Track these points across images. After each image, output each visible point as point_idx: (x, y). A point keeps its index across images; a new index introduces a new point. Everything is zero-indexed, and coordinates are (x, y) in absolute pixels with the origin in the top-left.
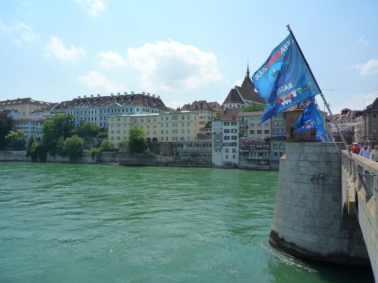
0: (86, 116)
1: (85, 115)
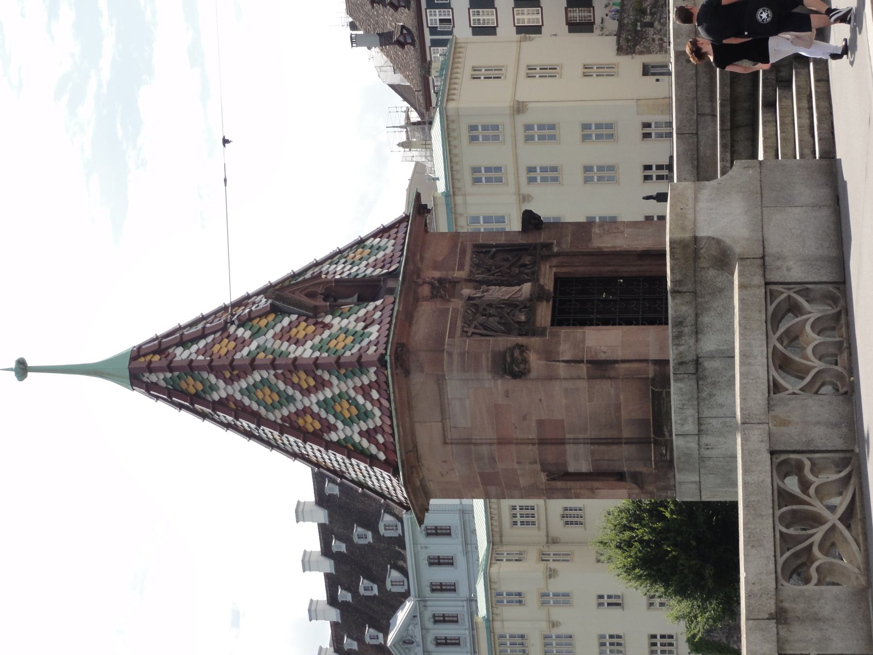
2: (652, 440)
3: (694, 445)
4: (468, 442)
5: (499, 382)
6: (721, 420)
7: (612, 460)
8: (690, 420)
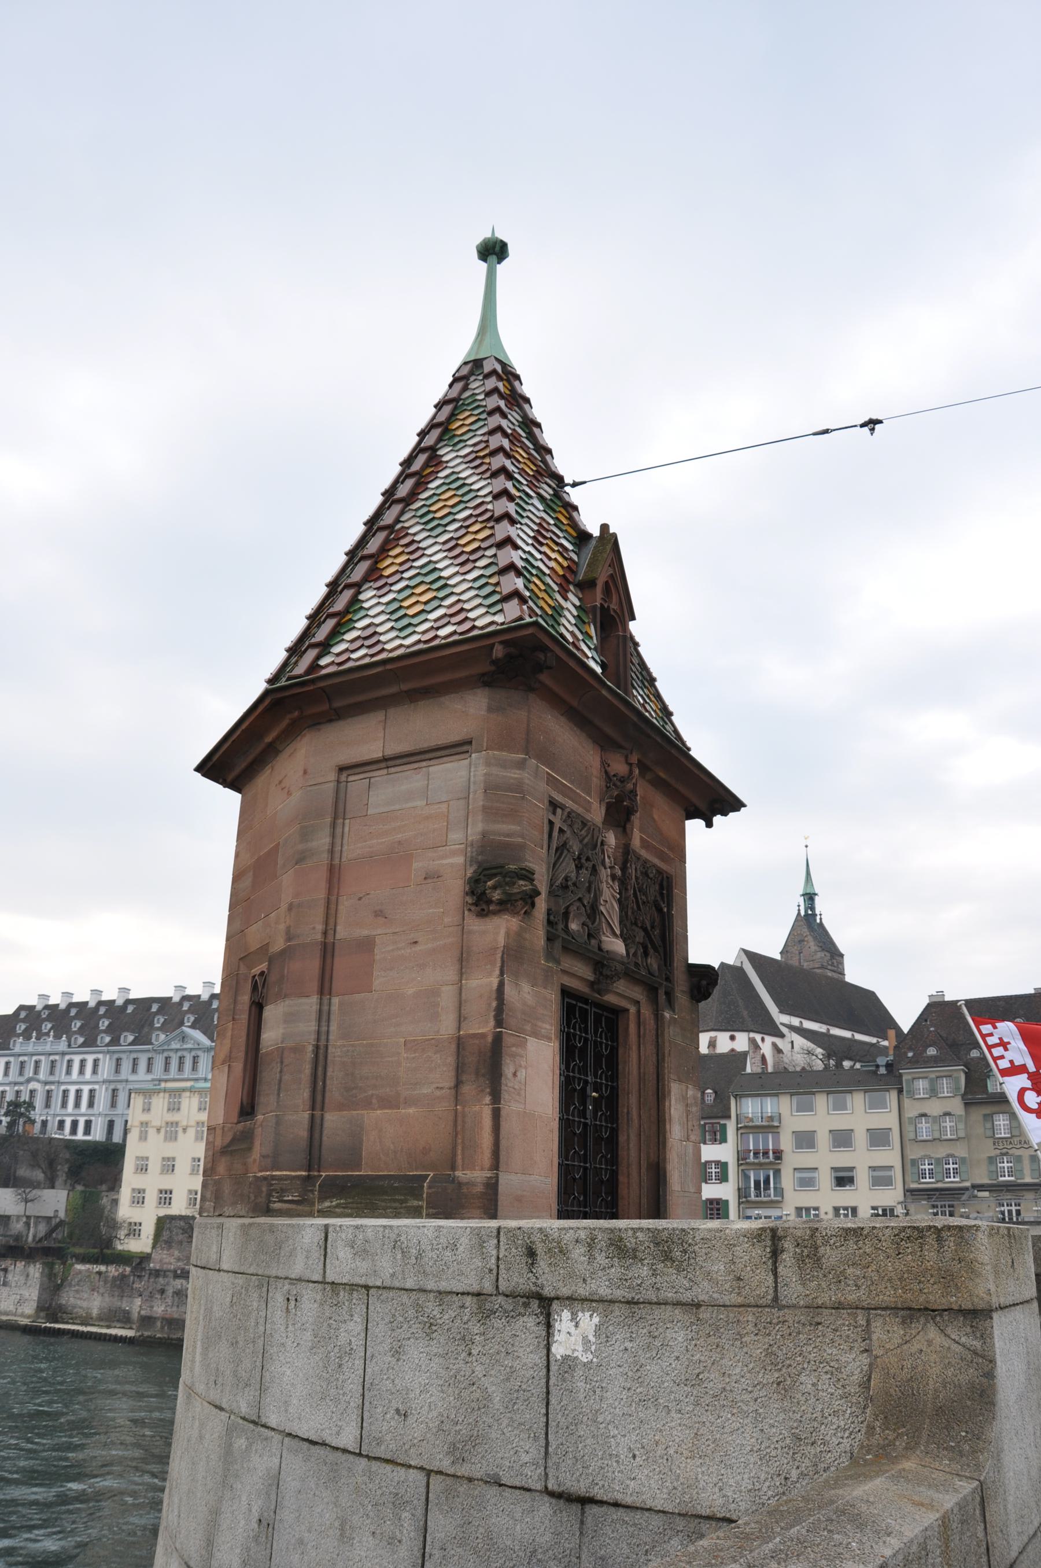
0: (53, 1087)
1: (51, 1078)
2: (316, 1173)
3: (298, 1269)
4: (339, 811)
5: (460, 860)
6: (357, 1343)
7: (279, 1089)
8: (363, 1266)
